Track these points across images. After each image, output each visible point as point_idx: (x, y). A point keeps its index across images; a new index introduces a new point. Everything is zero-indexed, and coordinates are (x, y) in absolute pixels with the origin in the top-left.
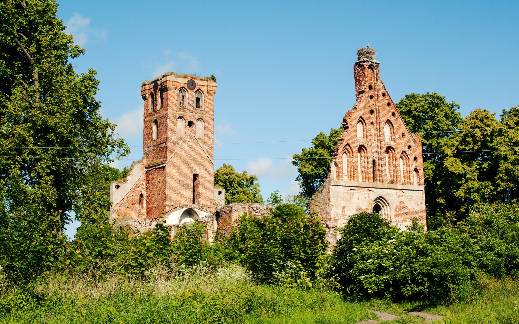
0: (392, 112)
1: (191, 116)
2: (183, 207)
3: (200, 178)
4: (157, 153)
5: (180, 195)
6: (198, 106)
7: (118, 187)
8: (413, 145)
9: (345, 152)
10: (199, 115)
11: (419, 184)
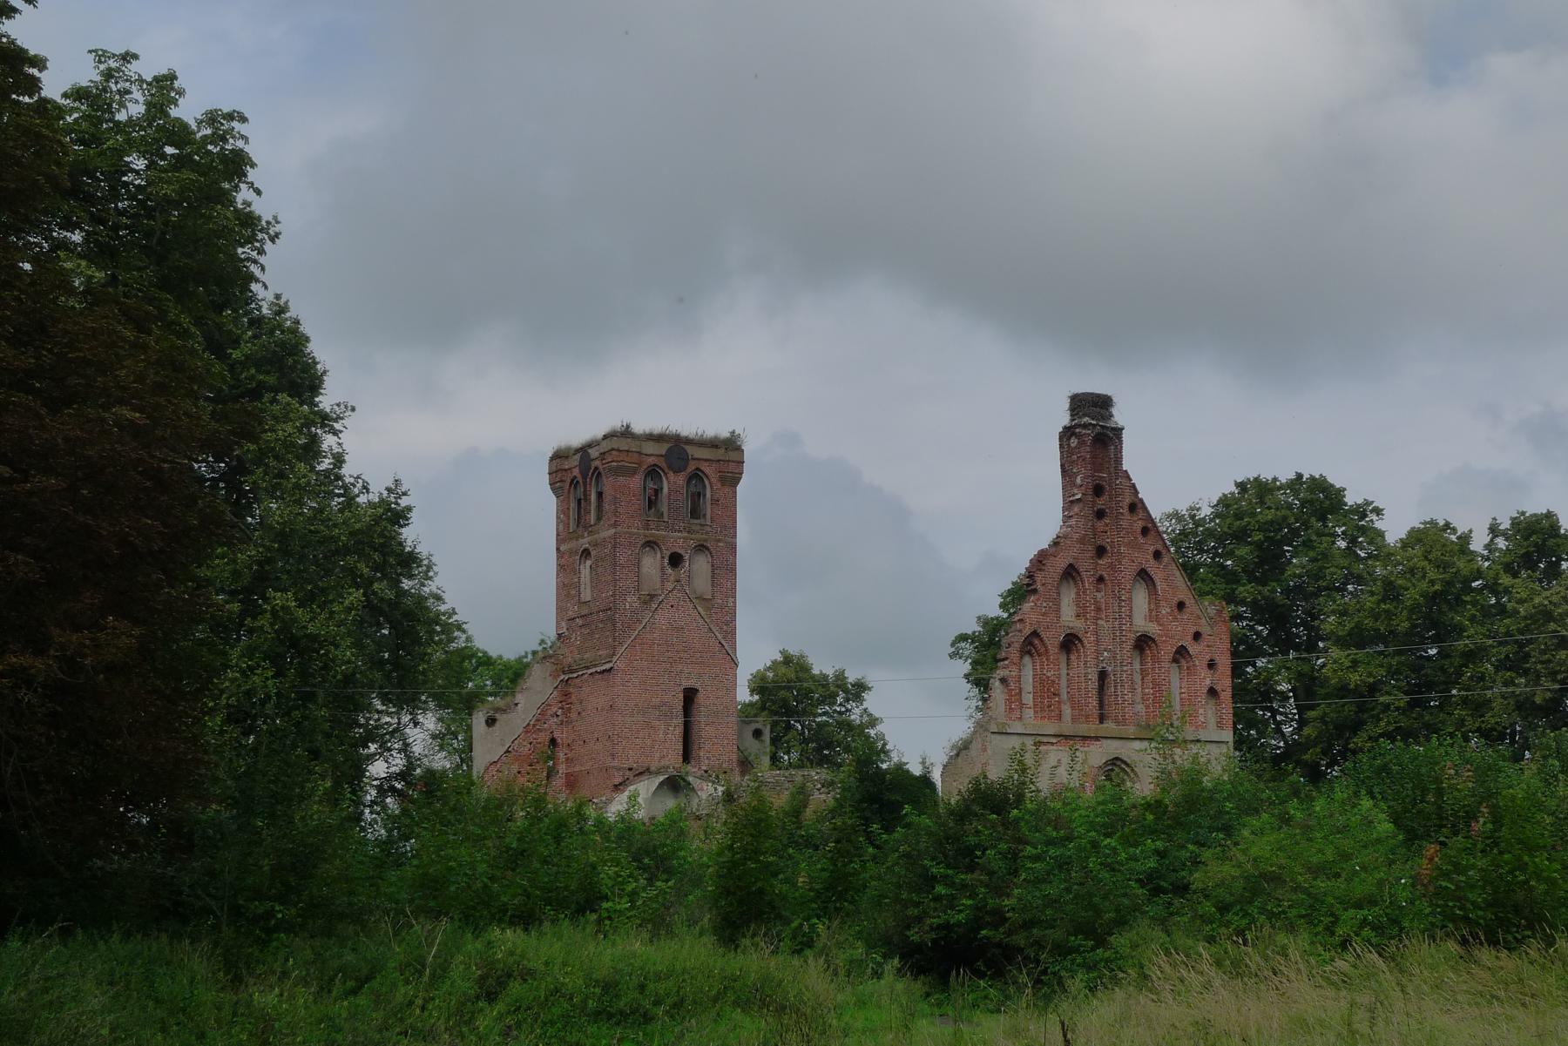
0: (1152, 549)
1: (677, 541)
2: (658, 773)
3: (700, 698)
4: (592, 633)
5: (649, 742)
6: (695, 512)
7: (491, 722)
8: (1205, 630)
9: (1029, 653)
10: (698, 536)
11: (1220, 725)
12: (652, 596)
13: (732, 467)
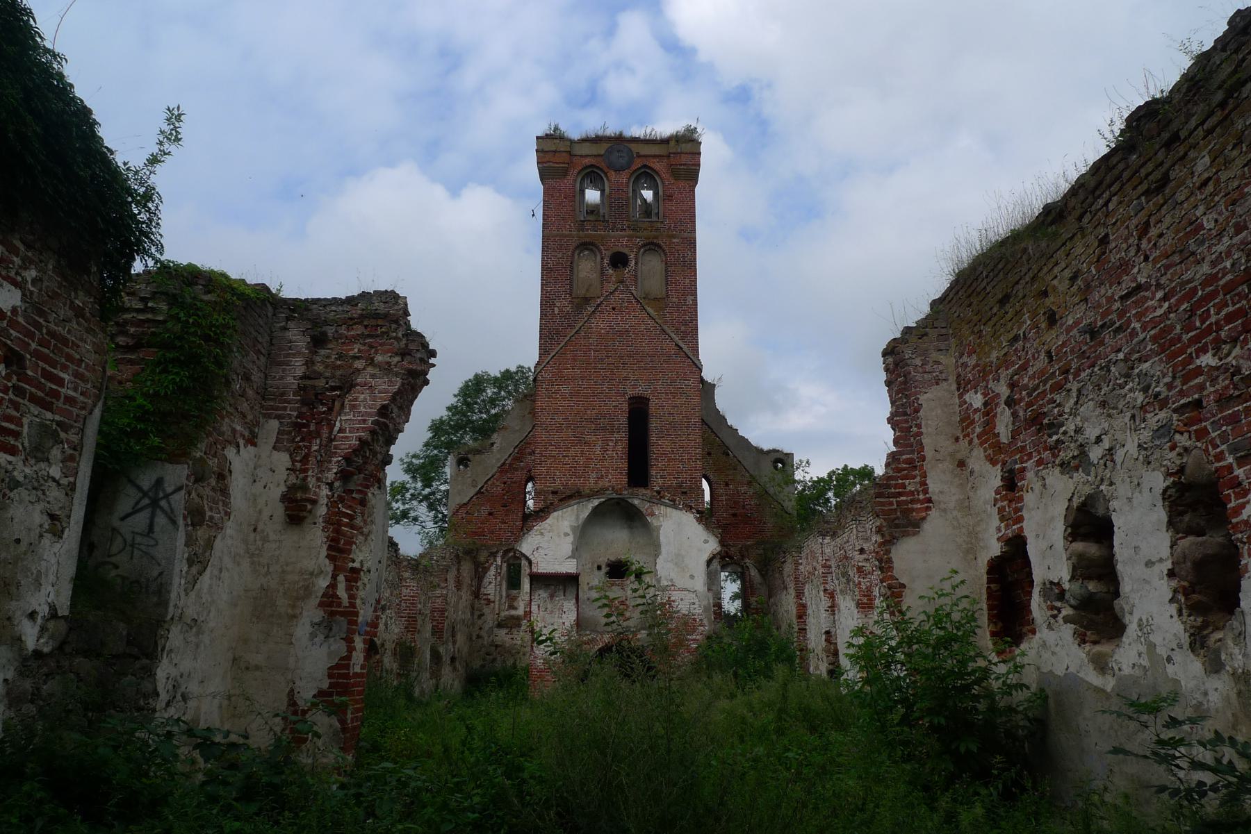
2: (590, 496)
5: (582, 461)
12: (587, 300)
13: (684, 159)
